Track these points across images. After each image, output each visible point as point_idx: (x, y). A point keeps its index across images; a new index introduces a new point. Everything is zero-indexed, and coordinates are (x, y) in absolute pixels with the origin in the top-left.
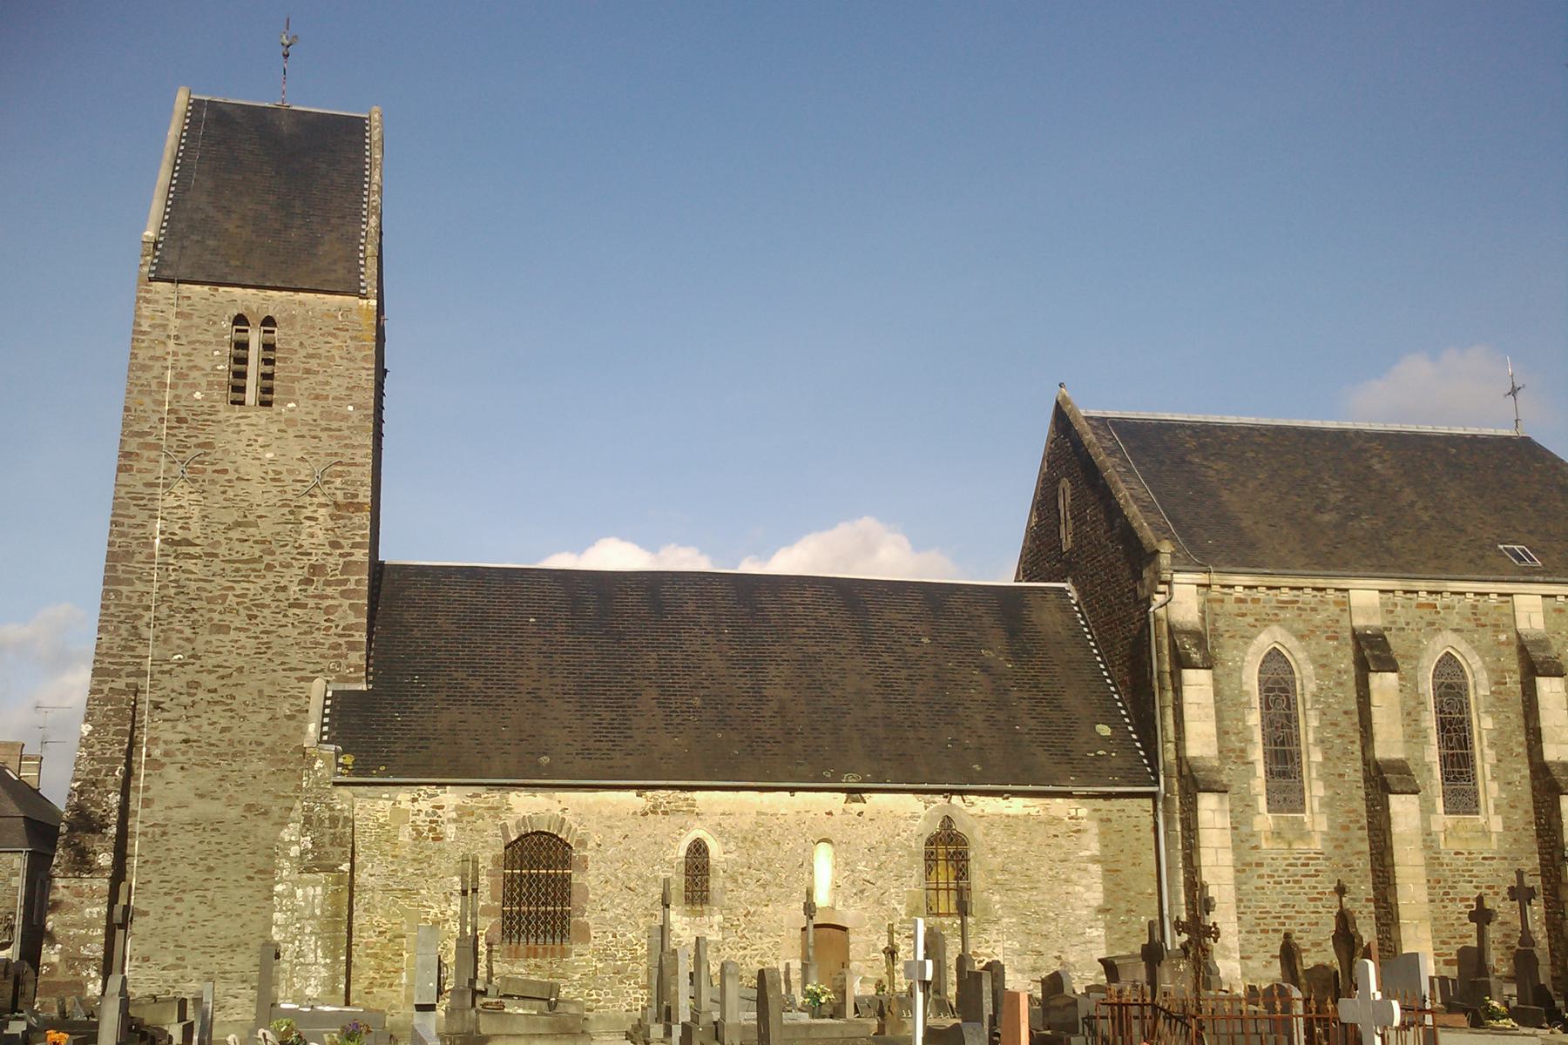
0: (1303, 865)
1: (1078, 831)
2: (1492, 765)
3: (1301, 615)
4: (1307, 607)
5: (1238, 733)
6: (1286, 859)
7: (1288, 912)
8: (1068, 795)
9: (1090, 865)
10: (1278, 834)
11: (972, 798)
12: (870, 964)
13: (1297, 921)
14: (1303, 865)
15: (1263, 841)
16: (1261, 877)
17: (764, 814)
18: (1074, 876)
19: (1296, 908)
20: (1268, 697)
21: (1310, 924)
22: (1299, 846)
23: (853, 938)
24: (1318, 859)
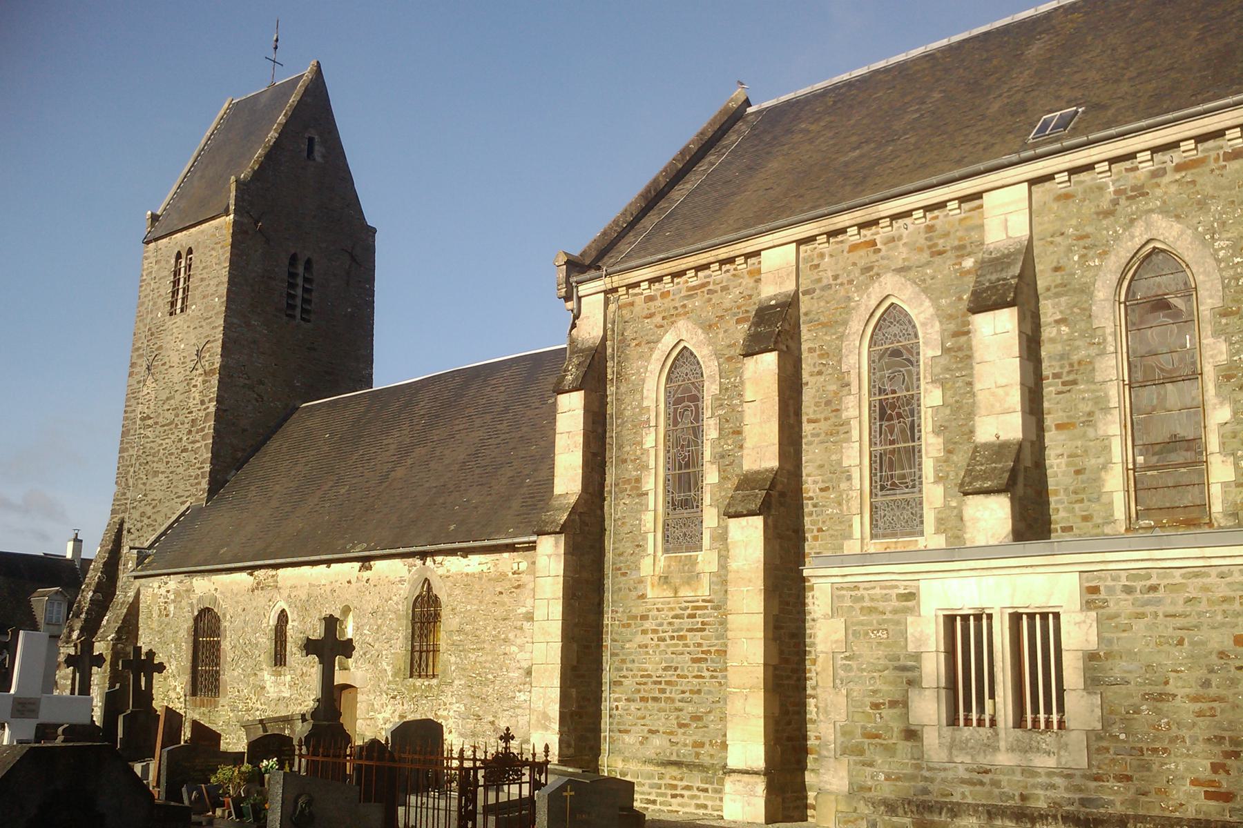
0: (690, 616)
1: (518, 587)
2: (937, 460)
3: (710, 300)
4: (718, 288)
5: (636, 460)
6: (672, 609)
7: (670, 676)
8: (511, 548)
9: (525, 623)
10: (665, 580)
11: (439, 559)
12: (368, 722)
13: (678, 687)
14: (690, 616)
15: (649, 588)
16: (644, 632)
17: (314, 586)
18: (511, 636)
19: (679, 672)
20: (675, 410)
21: (692, 692)
22: (685, 592)
23: (360, 697)
24: (706, 608)
